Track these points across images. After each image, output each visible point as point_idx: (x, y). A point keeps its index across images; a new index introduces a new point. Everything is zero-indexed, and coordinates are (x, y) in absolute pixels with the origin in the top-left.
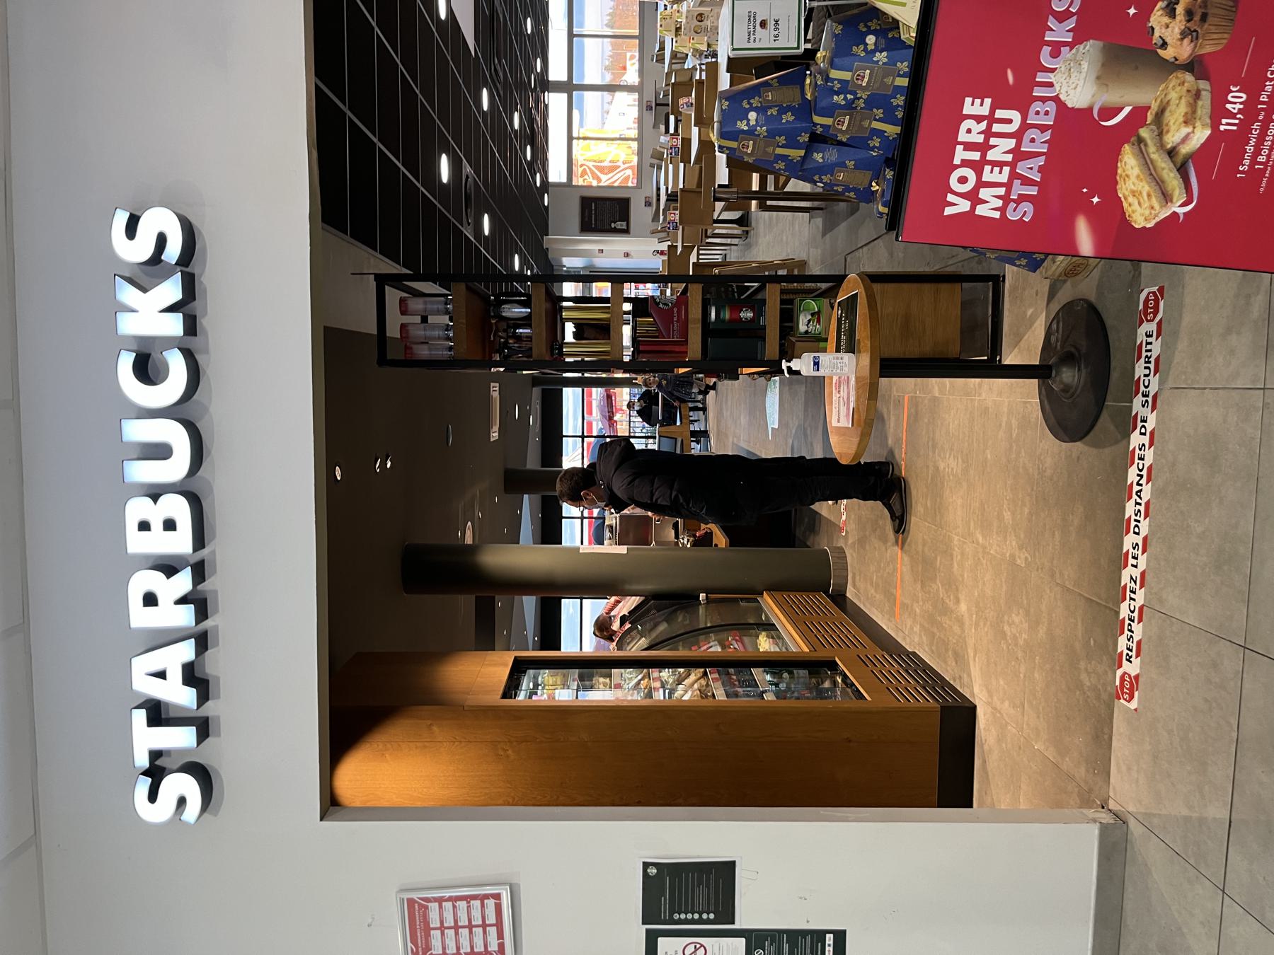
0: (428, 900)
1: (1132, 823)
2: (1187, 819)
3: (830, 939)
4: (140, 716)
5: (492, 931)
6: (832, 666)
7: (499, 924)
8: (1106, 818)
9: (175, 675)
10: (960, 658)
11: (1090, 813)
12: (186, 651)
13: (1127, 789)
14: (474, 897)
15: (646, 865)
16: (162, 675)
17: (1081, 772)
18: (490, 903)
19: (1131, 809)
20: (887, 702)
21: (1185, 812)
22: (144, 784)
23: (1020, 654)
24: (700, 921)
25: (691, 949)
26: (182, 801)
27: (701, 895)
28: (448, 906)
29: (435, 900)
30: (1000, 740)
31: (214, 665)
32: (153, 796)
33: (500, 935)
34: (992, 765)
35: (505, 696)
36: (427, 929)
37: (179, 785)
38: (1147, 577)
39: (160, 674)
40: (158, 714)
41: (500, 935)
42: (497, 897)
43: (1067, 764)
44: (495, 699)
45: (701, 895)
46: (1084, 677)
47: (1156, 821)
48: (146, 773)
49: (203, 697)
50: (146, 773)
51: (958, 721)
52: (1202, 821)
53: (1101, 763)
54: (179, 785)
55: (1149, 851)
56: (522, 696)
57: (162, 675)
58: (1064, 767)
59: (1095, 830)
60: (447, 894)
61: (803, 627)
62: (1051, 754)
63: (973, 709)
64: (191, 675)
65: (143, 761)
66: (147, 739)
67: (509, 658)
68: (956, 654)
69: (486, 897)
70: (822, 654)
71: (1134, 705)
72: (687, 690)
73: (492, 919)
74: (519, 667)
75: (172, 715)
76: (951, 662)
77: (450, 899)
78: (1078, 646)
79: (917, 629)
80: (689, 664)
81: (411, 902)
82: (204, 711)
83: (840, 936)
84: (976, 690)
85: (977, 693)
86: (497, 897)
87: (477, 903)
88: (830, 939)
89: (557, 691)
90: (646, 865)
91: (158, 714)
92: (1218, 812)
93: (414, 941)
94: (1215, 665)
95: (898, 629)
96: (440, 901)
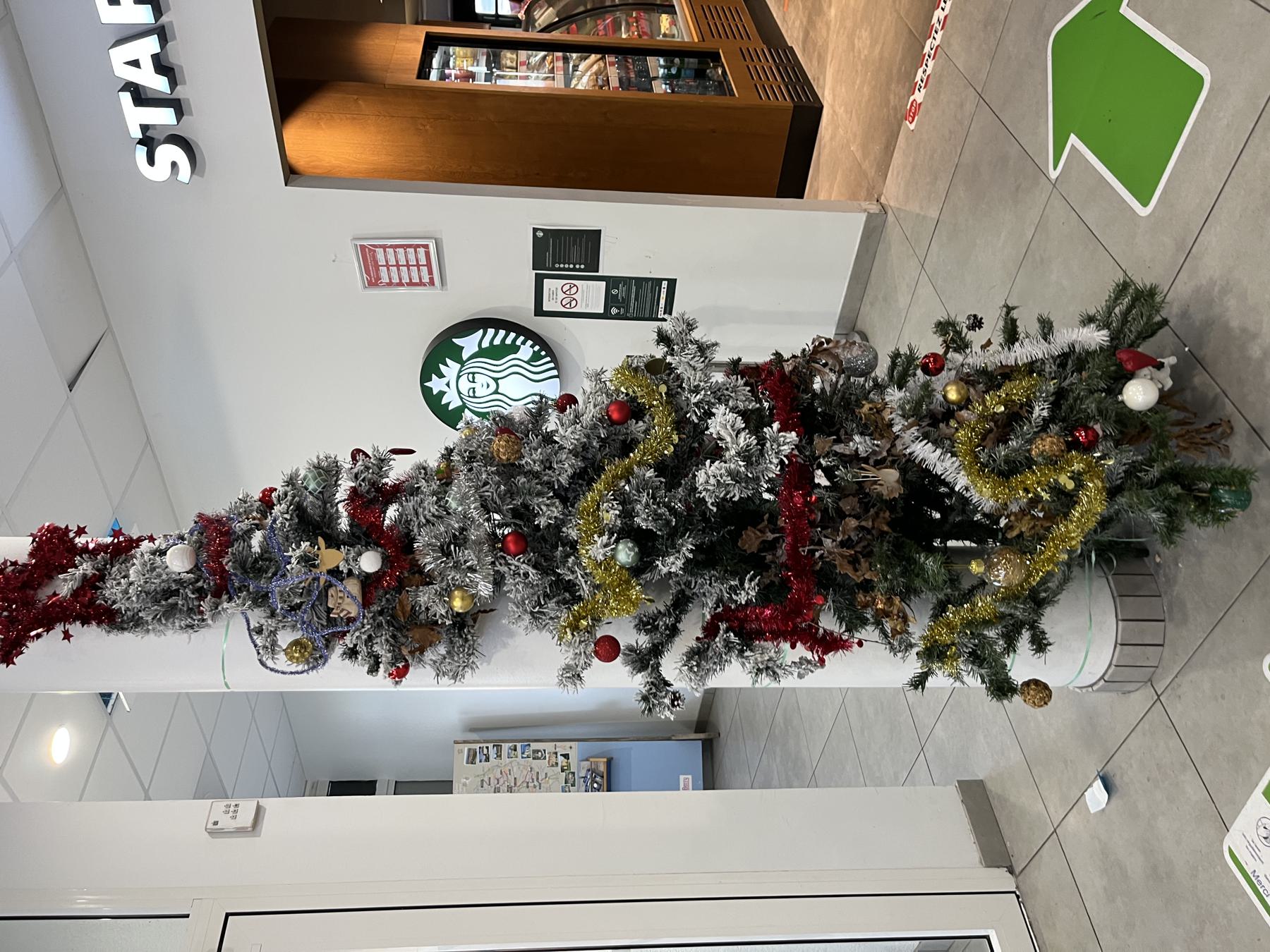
0: (375, 246)
1: (890, 213)
2: (918, 215)
3: (665, 284)
4: (126, 98)
5: (424, 269)
6: (715, 57)
7: (429, 265)
8: (874, 208)
9: (147, 64)
10: (821, 60)
11: (865, 205)
12: (151, 45)
13: (892, 192)
14: (410, 246)
15: (535, 230)
16: (135, 63)
17: (872, 173)
18: (421, 250)
19: (892, 204)
20: (753, 100)
21: (918, 210)
22: (141, 152)
23: (860, 68)
24: (574, 270)
25: (567, 287)
26: (174, 165)
27: (575, 253)
28: (390, 251)
29: (380, 246)
30: (832, 139)
31: (176, 56)
32: (151, 161)
33: (430, 272)
34: (822, 159)
35: (419, 77)
36: (377, 266)
37: (168, 153)
38: (948, 21)
39: (134, 61)
40: (141, 97)
41: (430, 272)
42: (426, 246)
43: (866, 165)
44: (411, 78)
45: (575, 253)
46: (892, 97)
47: (902, 215)
48: (141, 142)
49: (173, 84)
50: (141, 142)
51: (807, 116)
52: (924, 217)
53: (883, 167)
54: (168, 153)
55: (893, 231)
56: (434, 76)
57: (135, 63)
58: (864, 167)
59: (863, 217)
60: (389, 243)
61: (699, 12)
62: (858, 155)
63: (820, 109)
64: (162, 66)
65: (138, 134)
66: (136, 117)
67: (421, 32)
68: (819, 55)
69: (419, 246)
70: (709, 45)
71: (912, 127)
72: (585, 76)
73: (423, 261)
74: (432, 43)
75: (150, 96)
76: (815, 63)
77: (391, 246)
78: (895, 71)
79: (797, 23)
80: (585, 49)
81: (363, 247)
82: (174, 96)
83: (672, 283)
84: (826, 93)
85: (827, 97)
86: (426, 246)
87: (411, 250)
88: (665, 284)
89: (464, 66)
90: (535, 230)
91: (141, 97)
92: (933, 213)
93: (368, 272)
94: (962, 105)
95: (784, 20)
96: (384, 247)
